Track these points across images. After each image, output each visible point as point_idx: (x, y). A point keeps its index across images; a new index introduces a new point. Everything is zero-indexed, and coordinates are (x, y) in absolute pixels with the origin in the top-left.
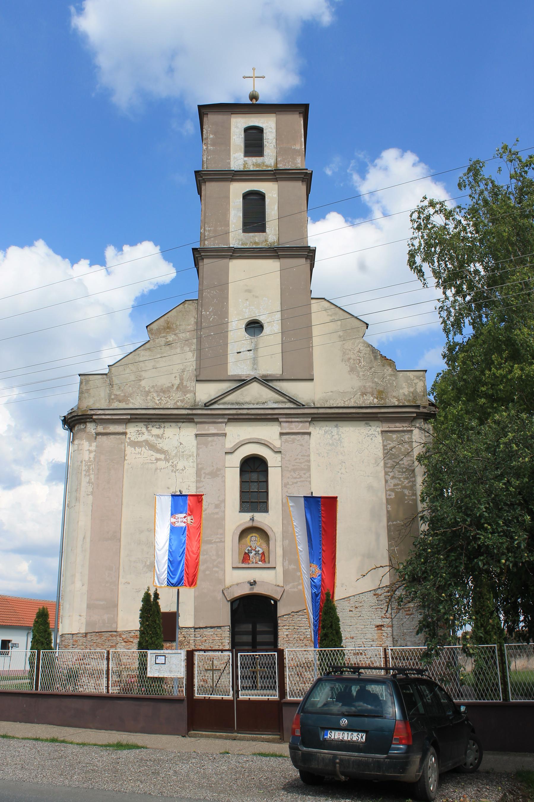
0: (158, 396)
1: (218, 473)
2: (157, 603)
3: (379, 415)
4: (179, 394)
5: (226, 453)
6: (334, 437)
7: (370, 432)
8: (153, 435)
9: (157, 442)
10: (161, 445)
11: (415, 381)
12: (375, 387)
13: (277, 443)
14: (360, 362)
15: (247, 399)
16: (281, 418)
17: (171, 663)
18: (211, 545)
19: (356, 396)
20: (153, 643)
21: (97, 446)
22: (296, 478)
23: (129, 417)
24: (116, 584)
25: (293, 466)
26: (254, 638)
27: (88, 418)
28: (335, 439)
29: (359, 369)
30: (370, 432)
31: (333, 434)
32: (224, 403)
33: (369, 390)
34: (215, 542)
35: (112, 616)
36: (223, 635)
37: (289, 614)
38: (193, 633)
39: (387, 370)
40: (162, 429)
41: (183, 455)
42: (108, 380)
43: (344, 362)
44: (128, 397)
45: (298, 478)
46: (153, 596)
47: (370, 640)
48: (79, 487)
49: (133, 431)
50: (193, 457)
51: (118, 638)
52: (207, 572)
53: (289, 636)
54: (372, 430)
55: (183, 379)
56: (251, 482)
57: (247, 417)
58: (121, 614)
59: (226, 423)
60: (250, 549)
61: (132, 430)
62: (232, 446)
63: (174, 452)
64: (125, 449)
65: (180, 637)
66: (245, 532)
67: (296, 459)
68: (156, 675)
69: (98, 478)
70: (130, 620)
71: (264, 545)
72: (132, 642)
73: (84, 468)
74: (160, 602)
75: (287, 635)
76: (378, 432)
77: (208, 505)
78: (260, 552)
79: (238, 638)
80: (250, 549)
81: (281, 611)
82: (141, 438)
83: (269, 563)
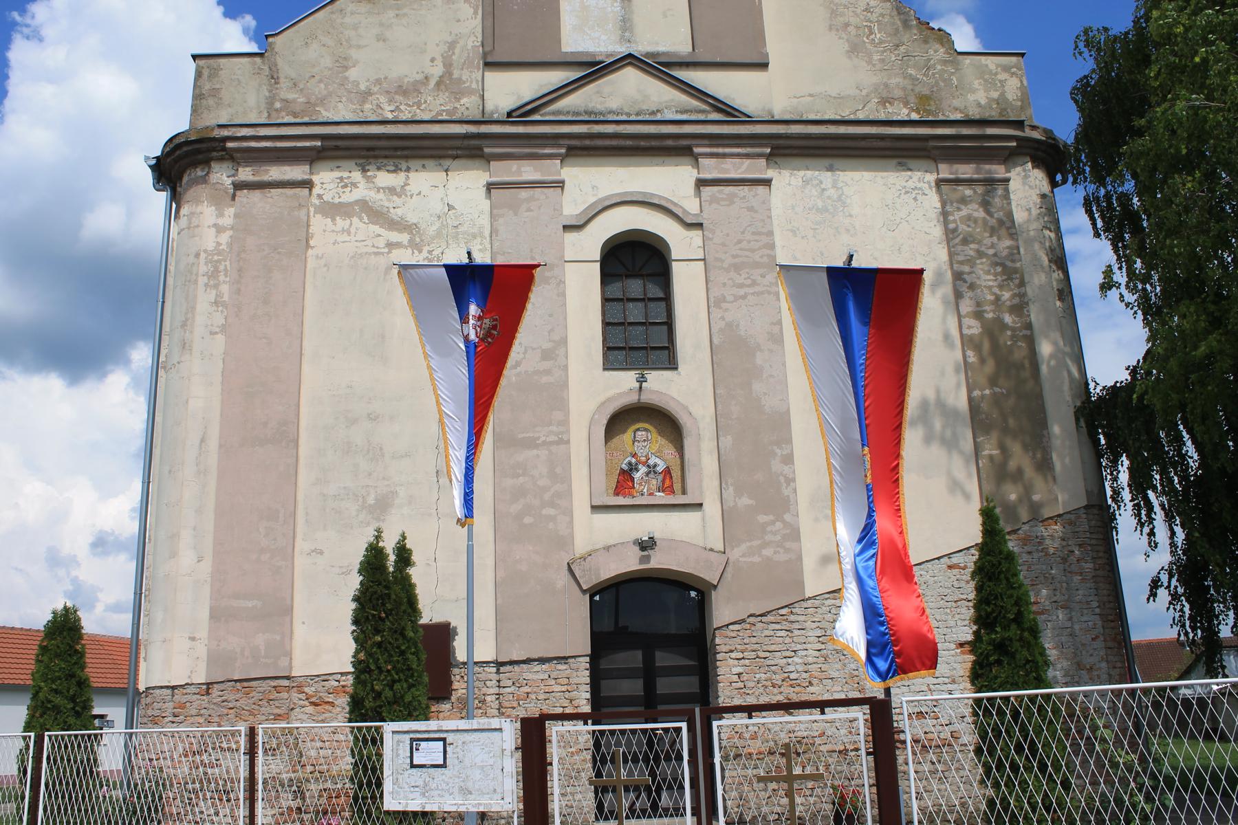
0: (390, 101)
2: (407, 578)
3: (932, 143)
4: (443, 97)
5: (564, 227)
6: (827, 193)
7: (910, 184)
8: (378, 189)
9: (391, 205)
10: (399, 212)
11: (999, 77)
12: (910, 87)
13: (690, 205)
14: (871, 33)
15: (614, 104)
16: (698, 146)
17: (467, 762)
18: (535, 452)
19: (869, 105)
20: (397, 700)
21: (236, 216)
22: (741, 286)
23: (319, 144)
24: (288, 554)
25: (734, 257)
26: (649, 686)
27: (214, 149)
28: (829, 198)
29: (869, 46)
30: (910, 184)
31: (823, 186)
32: (559, 112)
33: (898, 93)
34: (544, 443)
35: (278, 638)
36: (574, 680)
37: (743, 621)
38: (495, 677)
39: (936, 51)
40: (402, 175)
41: (457, 233)
42: (266, 68)
43: (834, 32)
44: (316, 105)
45: (749, 286)
46: (392, 558)
47: (947, 680)
48: (190, 315)
49: (328, 180)
50: (482, 237)
51: (295, 695)
52: (528, 520)
53: (745, 677)
54: (915, 179)
55: (451, 65)
56: (629, 300)
57: (614, 143)
58: (300, 631)
59: (563, 158)
60: (634, 460)
61: (327, 179)
62: (578, 212)
63: (434, 228)
64: (308, 220)
65: (459, 687)
66: (622, 419)
67: (740, 242)
68: (414, 806)
69: (238, 291)
70: (327, 644)
71: (670, 451)
72: (332, 704)
73: (203, 268)
74: (415, 574)
75: (739, 675)
76: (929, 182)
77: (525, 353)
78: (660, 469)
79: (608, 688)
80: (634, 460)
81: (722, 611)
82: (349, 196)
83: (684, 492)
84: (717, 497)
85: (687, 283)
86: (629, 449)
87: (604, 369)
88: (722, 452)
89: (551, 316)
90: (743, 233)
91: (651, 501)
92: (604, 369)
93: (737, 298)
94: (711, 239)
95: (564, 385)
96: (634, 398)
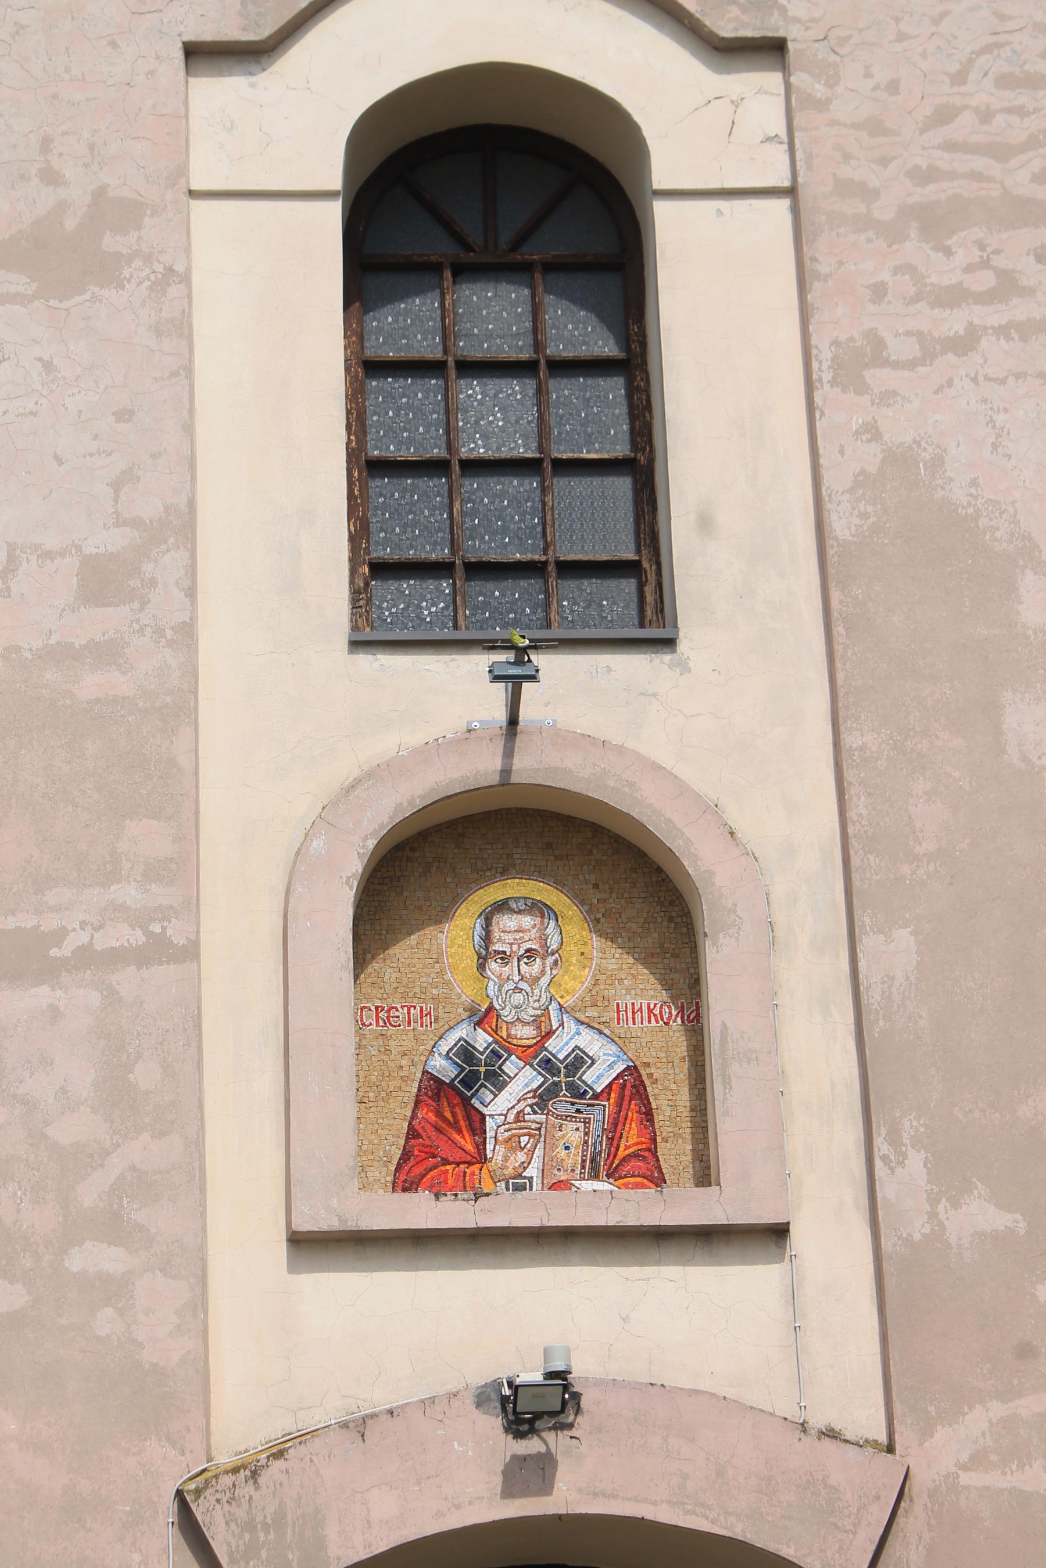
1: (111, 243)
18: (43, 995)
22: (952, 297)
25: (923, 176)
45: (986, 298)
56: (470, 368)
60: (482, 1040)
66: (426, 862)
67: (944, 116)
71: (641, 990)
80: (482, 1040)
83: (705, 1174)
84: (854, 1195)
85: (714, 284)
86: (466, 989)
87: (356, 645)
88: (873, 998)
89: (124, 415)
90: (959, 78)
91: (559, 1212)
92: (356, 645)
93: (931, 348)
94: (822, 105)
95: (180, 707)
96: (482, 766)
